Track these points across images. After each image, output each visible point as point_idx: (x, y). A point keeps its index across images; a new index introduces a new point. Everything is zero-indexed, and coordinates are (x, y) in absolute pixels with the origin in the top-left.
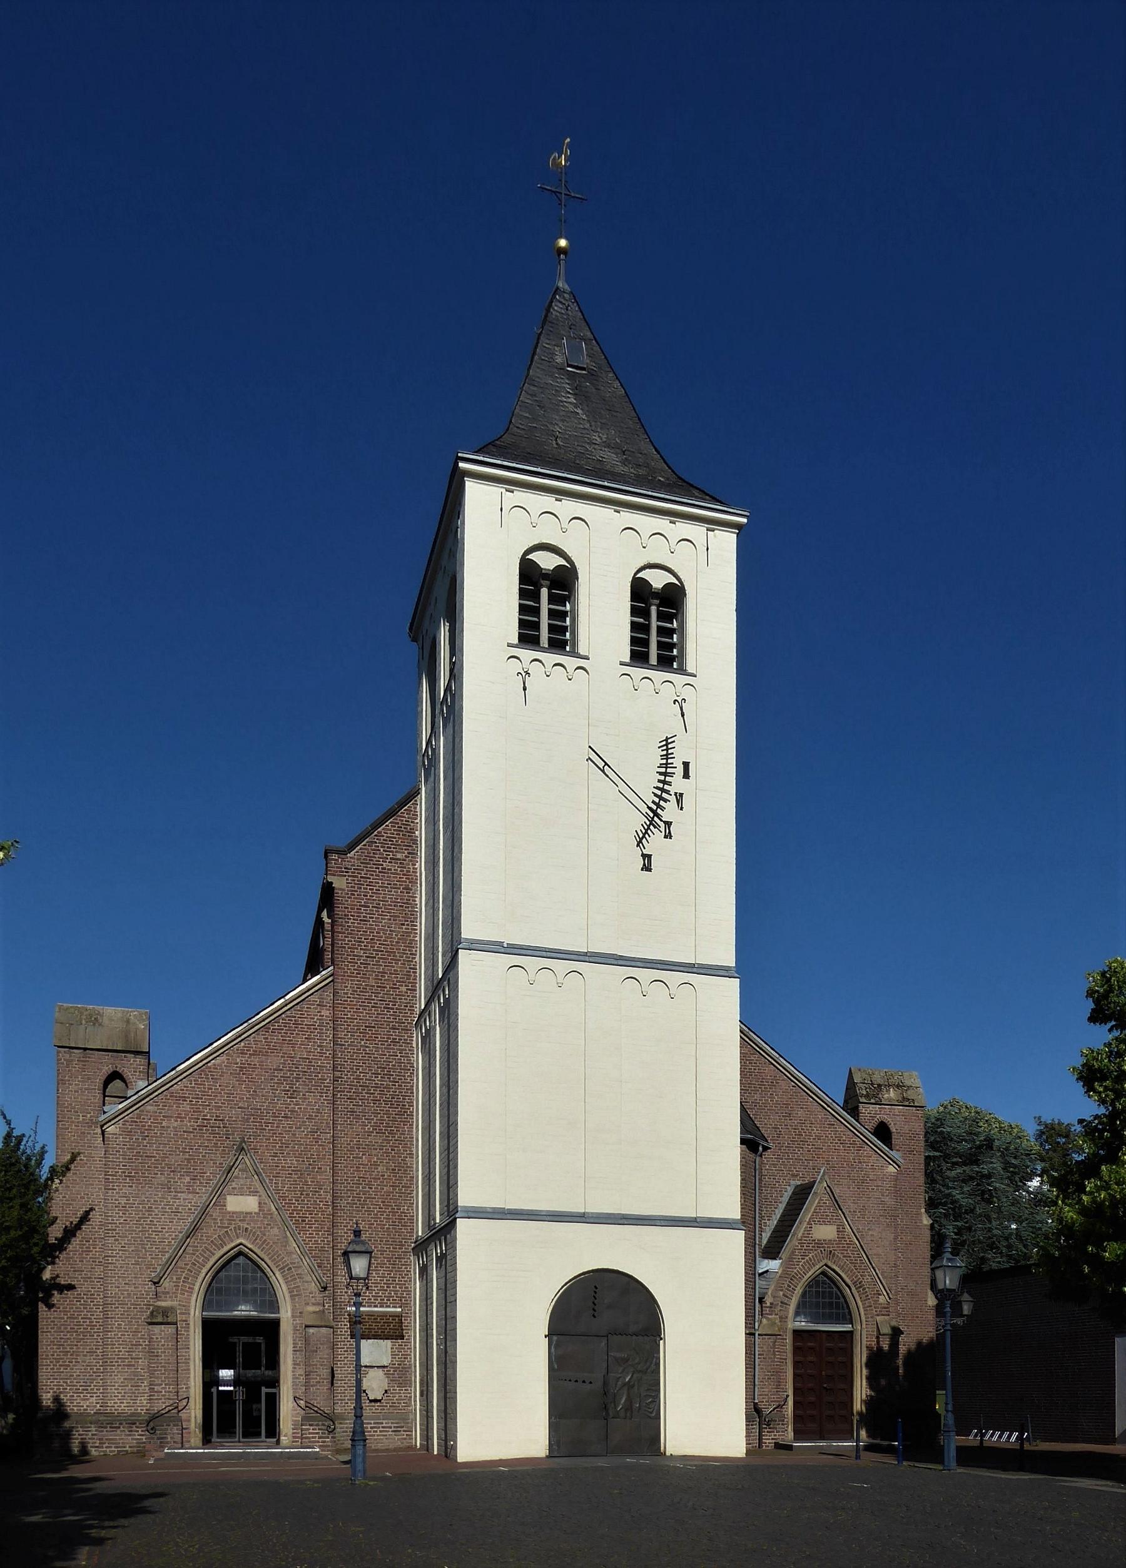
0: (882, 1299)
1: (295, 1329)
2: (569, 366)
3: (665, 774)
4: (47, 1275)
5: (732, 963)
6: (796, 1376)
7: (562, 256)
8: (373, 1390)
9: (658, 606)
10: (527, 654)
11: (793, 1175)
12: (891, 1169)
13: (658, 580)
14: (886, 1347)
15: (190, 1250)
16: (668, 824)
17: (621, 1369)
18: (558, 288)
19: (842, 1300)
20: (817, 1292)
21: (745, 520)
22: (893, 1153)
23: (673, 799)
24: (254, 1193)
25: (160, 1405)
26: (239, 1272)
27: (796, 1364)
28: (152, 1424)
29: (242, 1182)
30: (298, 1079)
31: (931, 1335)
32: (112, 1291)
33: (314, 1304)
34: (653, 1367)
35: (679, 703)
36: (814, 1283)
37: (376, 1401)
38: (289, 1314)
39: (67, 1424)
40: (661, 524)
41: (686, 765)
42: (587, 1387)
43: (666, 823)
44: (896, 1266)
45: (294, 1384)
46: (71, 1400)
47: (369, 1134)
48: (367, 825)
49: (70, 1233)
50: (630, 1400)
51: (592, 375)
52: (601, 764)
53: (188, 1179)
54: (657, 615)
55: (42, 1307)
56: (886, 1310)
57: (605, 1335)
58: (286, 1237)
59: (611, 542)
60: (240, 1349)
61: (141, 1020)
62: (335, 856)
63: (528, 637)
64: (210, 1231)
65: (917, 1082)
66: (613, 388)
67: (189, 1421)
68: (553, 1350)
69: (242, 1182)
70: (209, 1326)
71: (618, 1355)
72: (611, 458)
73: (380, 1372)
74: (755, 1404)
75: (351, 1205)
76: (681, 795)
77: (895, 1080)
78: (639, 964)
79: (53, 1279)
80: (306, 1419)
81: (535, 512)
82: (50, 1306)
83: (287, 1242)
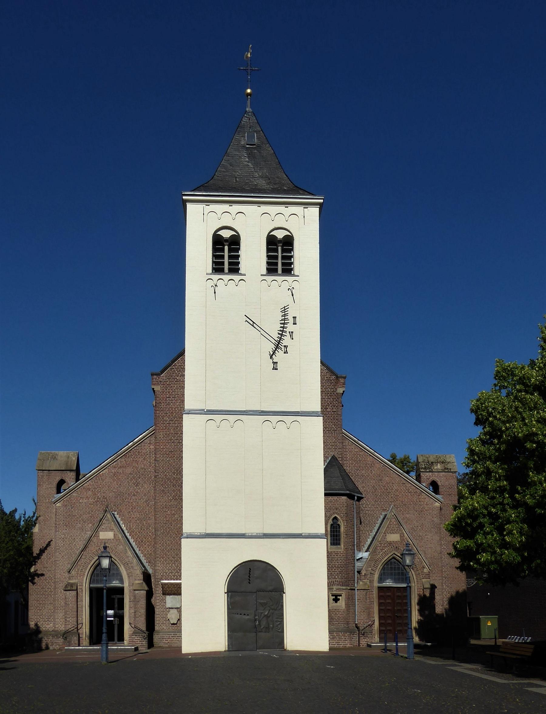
0: (425, 570)
1: (130, 592)
2: (247, 145)
3: (284, 324)
4: (32, 570)
5: (319, 409)
6: (380, 611)
7: (249, 97)
8: (172, 619)
10: (216, 277)
11: (384, 510)
12: (437, 504)
13: (280, 235)
14: (428, 595)
15: (83, 557)
20: (391, 568)
21: (322, 201)
23: (288, 334)
24: (112, 530)
27: (380, 604)
28: (65, 636)
29: (106, 525)
30: (139, 477)
31: (464, 588)
32: (58, 576)
34: (280, 607)
36: (388, 563)
37: (174, 624)
38: (127, 585)
39: (40, 636)
40: (281, 208)
41: (294, 318)
42: (247, 617)
43: (285, 346)
44: (441, 553)
45: (130, 617)
46: (42, 625)
48: (169, 361)
49: (42, 551)
51: (259, 147)
53: (91, 525)
54: (280, 253)
55: (30, 584)
56: (428, 576)
57: (255, 593)
59: (254, 221)
60: (116, 601)
61: (74, 456)
62: (155, 377)
63: (218, 268)
66: (268, 150)
67: (83, 634)
69: (106, 525)
70: (91, 590)
71: (262, 601)
72: (262, 183)
73: (176, 610)
74: (356, 624)
75: (163, 534)
76: (292, 332)
77: (442, 459)
78: (271, 414)
79: (35, 571)
80: (134, 633)
81: (219, 213)
82: (34, 583)
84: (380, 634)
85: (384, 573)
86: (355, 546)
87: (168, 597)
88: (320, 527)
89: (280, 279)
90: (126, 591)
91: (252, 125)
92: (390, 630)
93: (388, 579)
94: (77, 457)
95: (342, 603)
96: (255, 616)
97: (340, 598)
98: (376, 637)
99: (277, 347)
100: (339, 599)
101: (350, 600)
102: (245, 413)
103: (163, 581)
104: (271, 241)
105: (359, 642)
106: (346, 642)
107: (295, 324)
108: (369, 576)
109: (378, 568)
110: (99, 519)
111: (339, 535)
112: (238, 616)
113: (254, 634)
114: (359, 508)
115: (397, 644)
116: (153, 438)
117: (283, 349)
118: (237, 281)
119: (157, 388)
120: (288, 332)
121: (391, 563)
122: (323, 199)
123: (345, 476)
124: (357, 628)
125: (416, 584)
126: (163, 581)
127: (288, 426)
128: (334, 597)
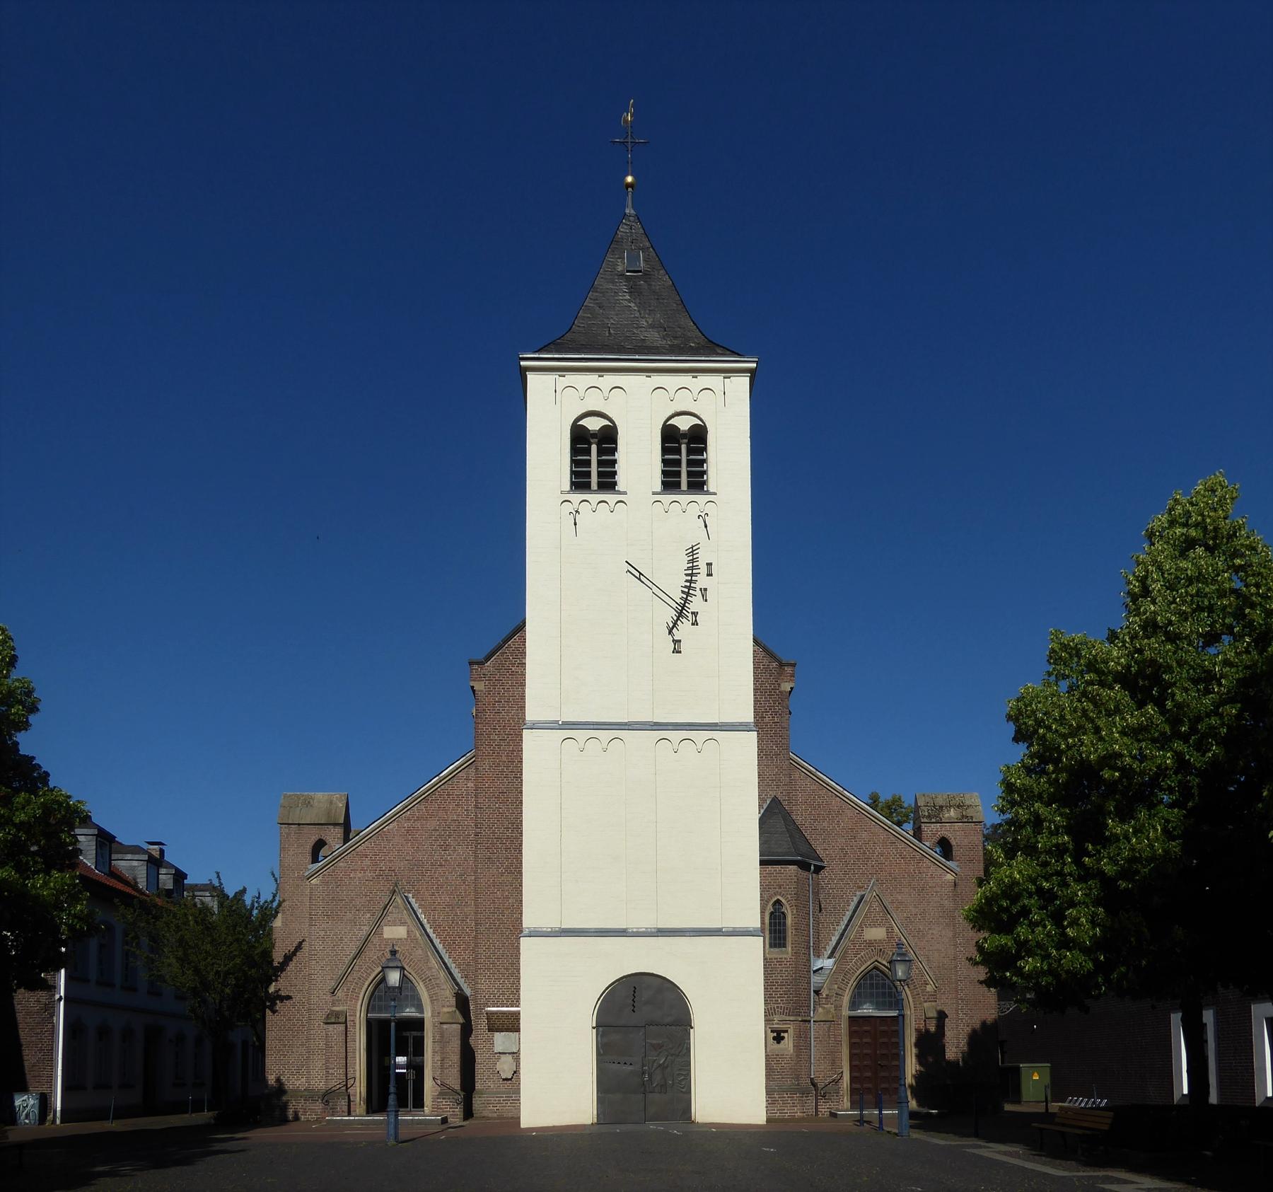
3: (692, 575)
4: (272, 989)
6: (852, 1056)
9: (688, 444)
10: (577, 497)
12: (949, 877)
13: (684, 424)
14: (933, 1029)
15: (357, 968)
16: (695, 614)
22: (949, 863)
23: (698, 593)
24: (403, 923)
25: (334, 1083)
27: (852, 1046)
30: (449, 836)
35: (703, 517)
36: (866, 975)
39: (284, 1098)
42: (631, 1068)
47: (502, 875)
48: (500, 641)
49: (288, 958)
51: (646, 275)
54: (684, 455)
56: (933, 997)
57: (643, 1026)
59: (642, 403)
60: (411, 1041)
63: (580, 482)
64: (372, 954)
65: (978, 801)
66: (662, 280)
70: (369, 1023)
72: (654, 337)
75: (488, 929)
82: (274, 1012)
87: (497, 1035)
95: (788, 1043)
99: (680, 614)
100: (783, 1038)
107: (710, 575)
111: (785, 931)
116: (472, 770)
119: (479, 686)
123: (795, 831)
124: (814, 1085)
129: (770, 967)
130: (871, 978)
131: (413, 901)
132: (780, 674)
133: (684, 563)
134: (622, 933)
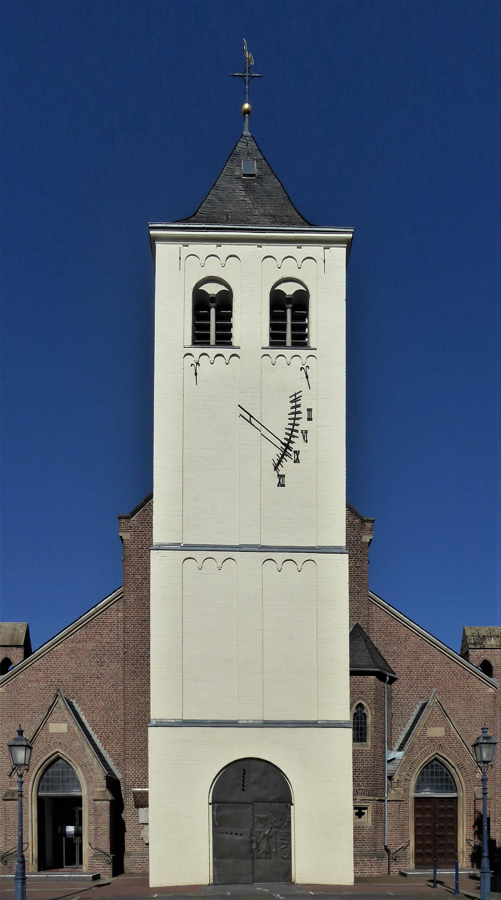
6: (416, 828)
7: (247, 115)
9: (293, 309)
10: (197, 351)
12: (491, 690)
16: (297, 453)
17: (262, 826)
18: (243, 135)
19: (450, 777)
20: (432, 772)
21: (351, 235)
23: (299, 434)
24: (65, 721)
26: (55, 768)
27: (417, 820)
30: (104, 655)
33: (100, 787)
34: (286, 824)
36: (427, 766)
41: (310, 410)
42: (240, 838)
43: (295, 452)
45: (89, 835)
50: (269, 846)
52: (248, 417)
54: (289, 316)
57: (251, 803)
58: (84, 747)
59: (251, 271)
63: (200, 337)
67: (28, 857)
68: (215, 813)
70: (41, 801)
71: (261, 816)
74: (386, 846)
76: (306, 432)
83: (84, 750)
84: (415, 859)
85: (423, 780)
86: (384, 743)
88: (345, 714)
89: (289, 353)
90: (85, 802)
91: (250, 152)
92: (429, 853)
93: (427, 787)
94: (25, 629)
95: (368, 818)
96: (252, 836)
97: (365, 811)
98: (411, 862)
99: (285, 453)
100: (364, 813)
101: (379, 813)
102: (238, 549)
103: (135, 789)
104: (278, 301)
105: (389, 869)
106: (373, 870)
107: (310, 419)
108: (403, 783)
109: (416, 772)
110: (48, 707)
111: (365, 729)
112: (227, 837)
113: (249, 862)
114: (390, 692)
115: (435, 872)
116: (121, 603)
117: (293, 457)
118: (227, 357)
119: (126, 536)
120: (300, 432)
121: (432, 766)
122: (353, 233)
123: (373, 651)
124: (387, 850)
125: (465, 794)
126: (135, 789)
127: (300, 566)
128: (357, 811)
129: (356, 756)
130: (432, 766)
131: (76, 705)
132: (362, 528)
133: (288, 407)
134: (234, 724)
